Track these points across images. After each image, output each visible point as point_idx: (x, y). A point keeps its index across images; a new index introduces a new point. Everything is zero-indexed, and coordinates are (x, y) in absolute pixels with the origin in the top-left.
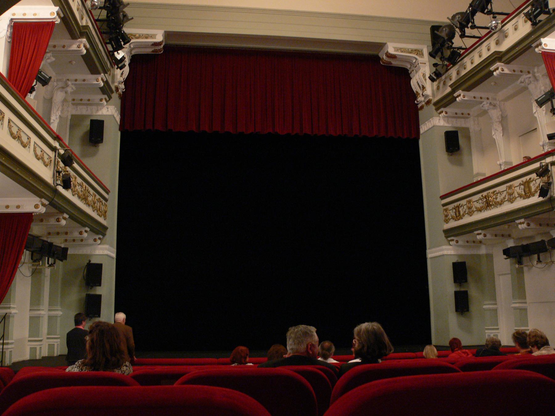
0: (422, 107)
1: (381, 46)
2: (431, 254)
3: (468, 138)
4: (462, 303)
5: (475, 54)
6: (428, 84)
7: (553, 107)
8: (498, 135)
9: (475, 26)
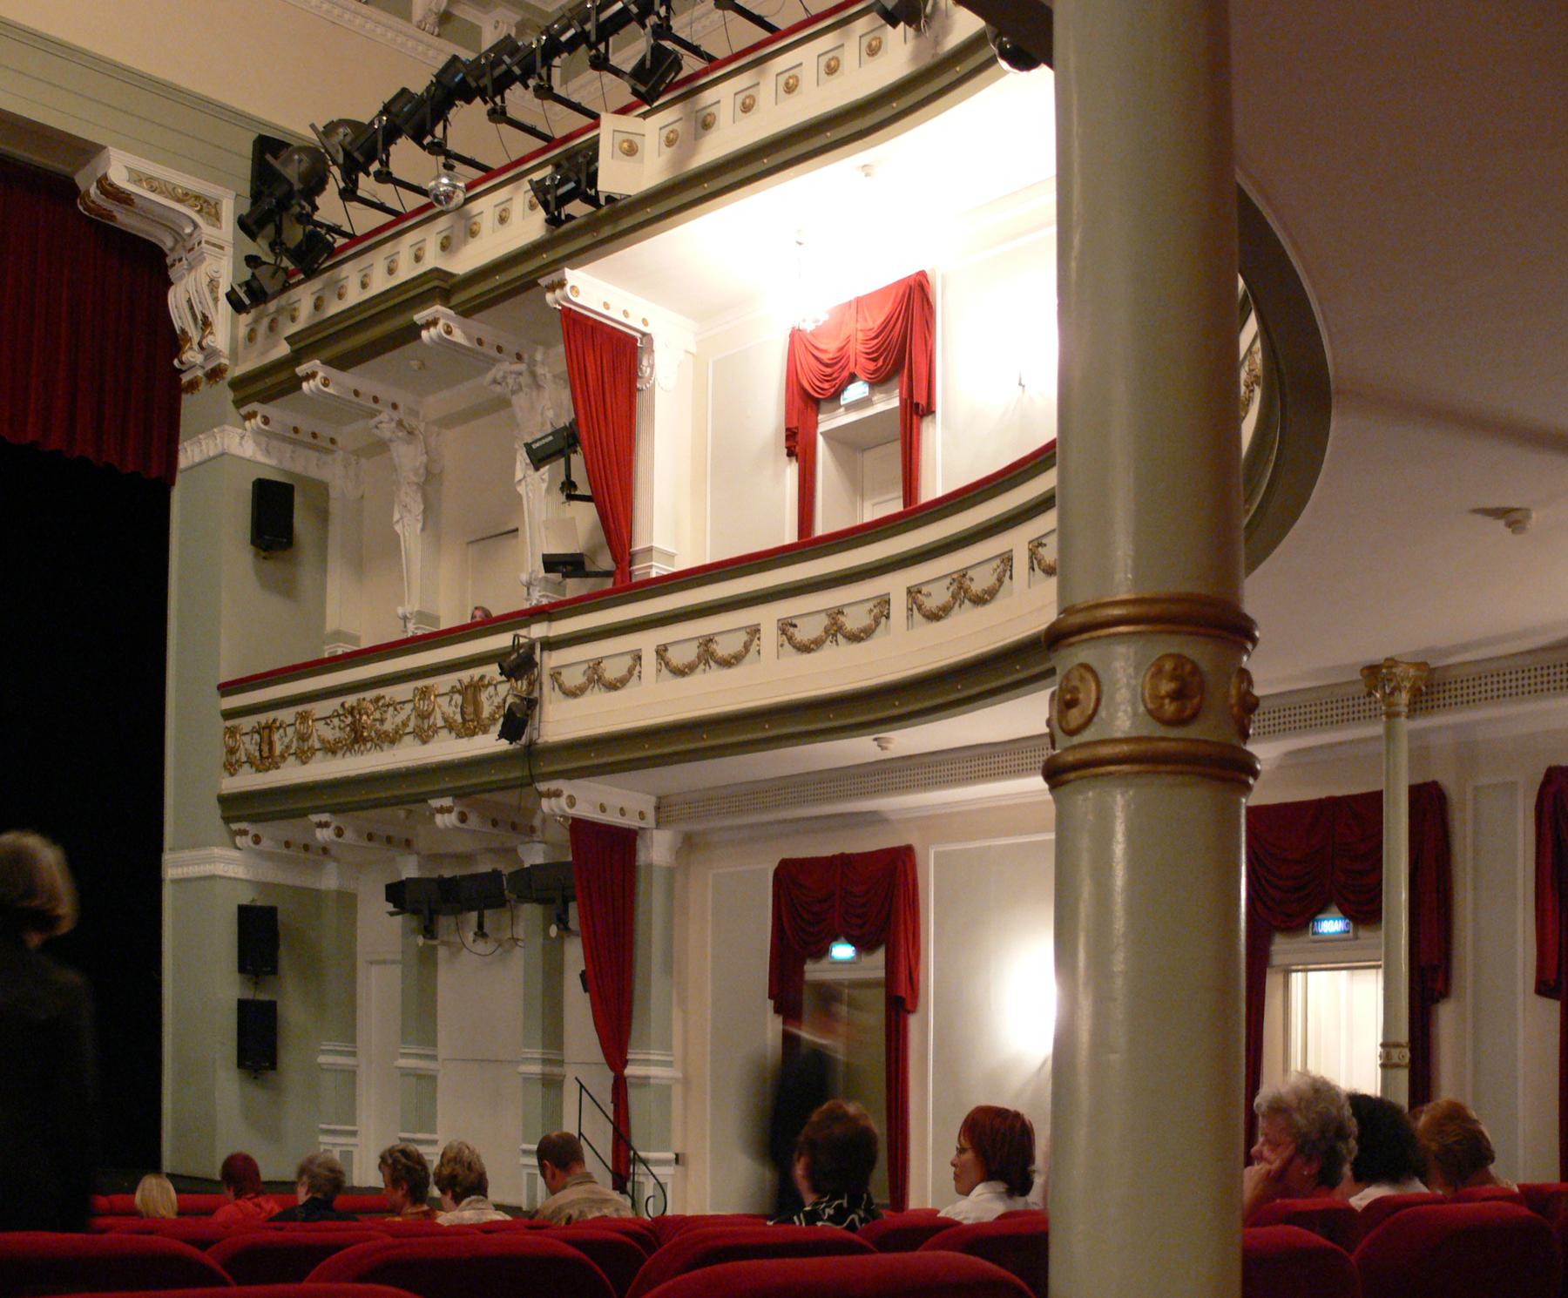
0: (193, 385)
1: (88, 151)
2: (176, 865)
3: (323, 515)
4: (258, 1040)
5: (377, 262)
6: (222, 313)
7: (568, 476)
8: (408, 527)
9: (389, 174)
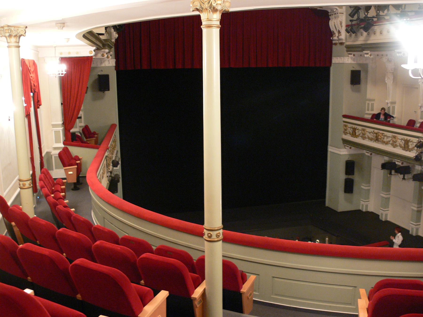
0: (336, 44)
4: (349, 187)
